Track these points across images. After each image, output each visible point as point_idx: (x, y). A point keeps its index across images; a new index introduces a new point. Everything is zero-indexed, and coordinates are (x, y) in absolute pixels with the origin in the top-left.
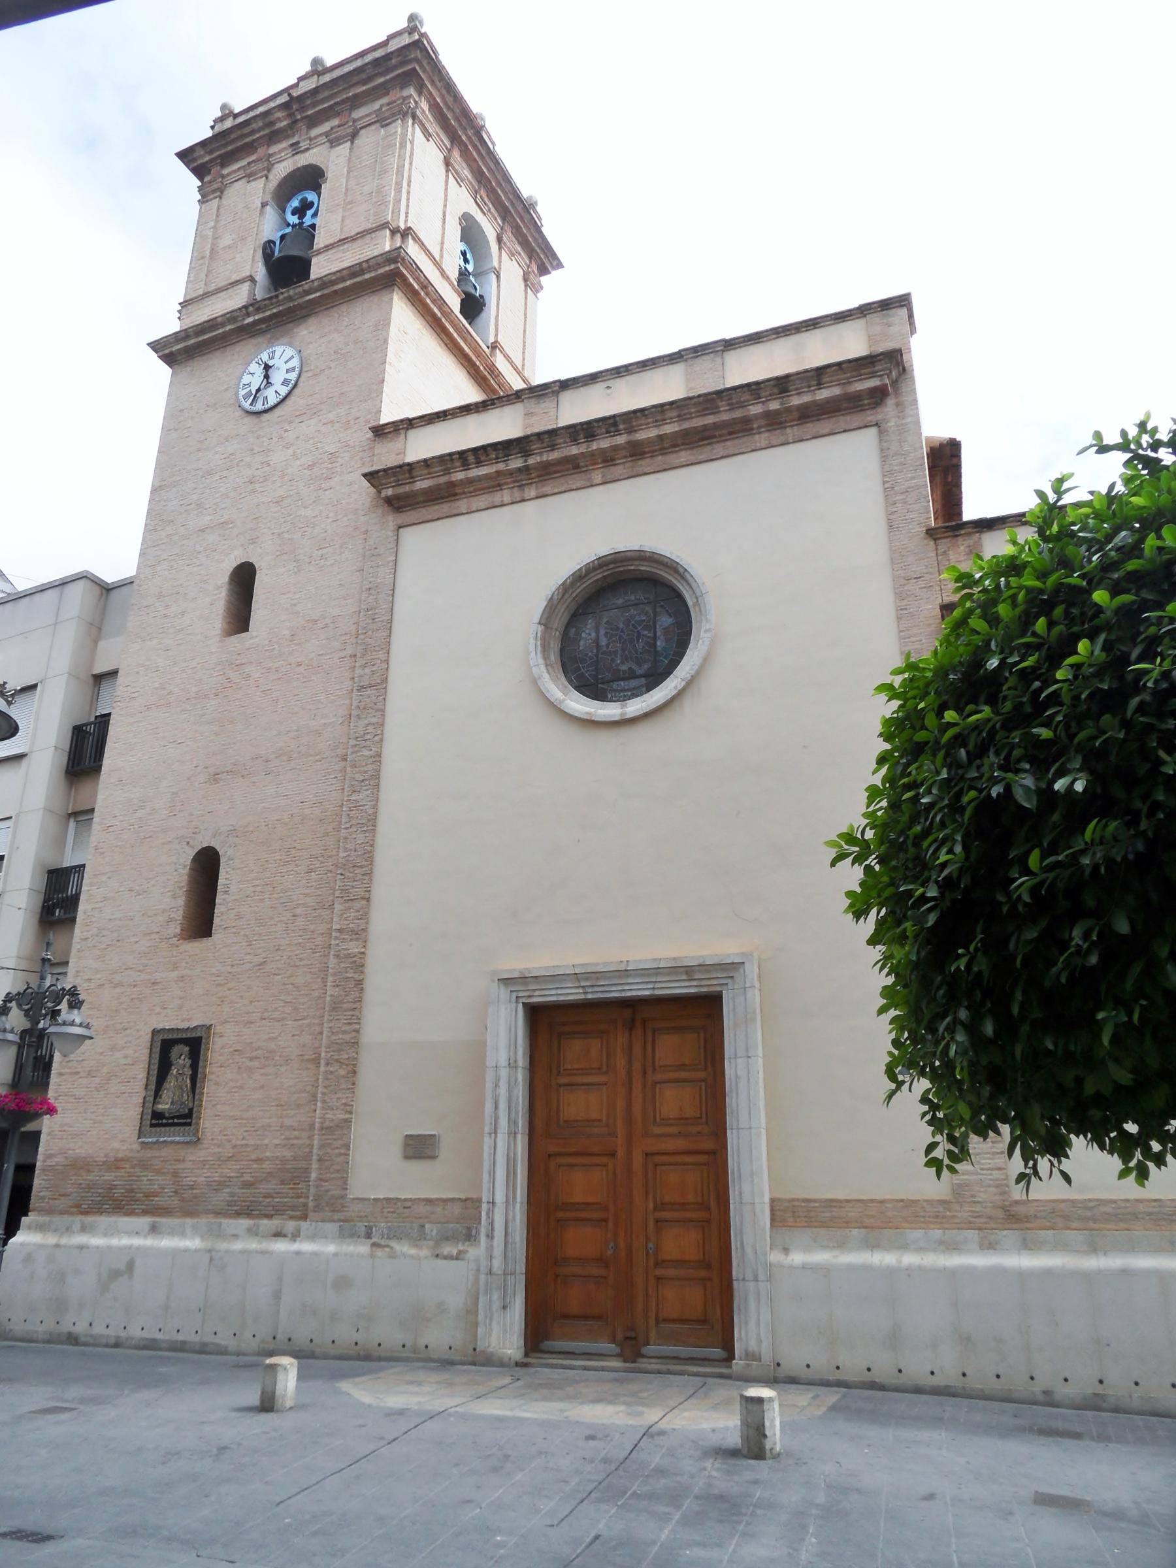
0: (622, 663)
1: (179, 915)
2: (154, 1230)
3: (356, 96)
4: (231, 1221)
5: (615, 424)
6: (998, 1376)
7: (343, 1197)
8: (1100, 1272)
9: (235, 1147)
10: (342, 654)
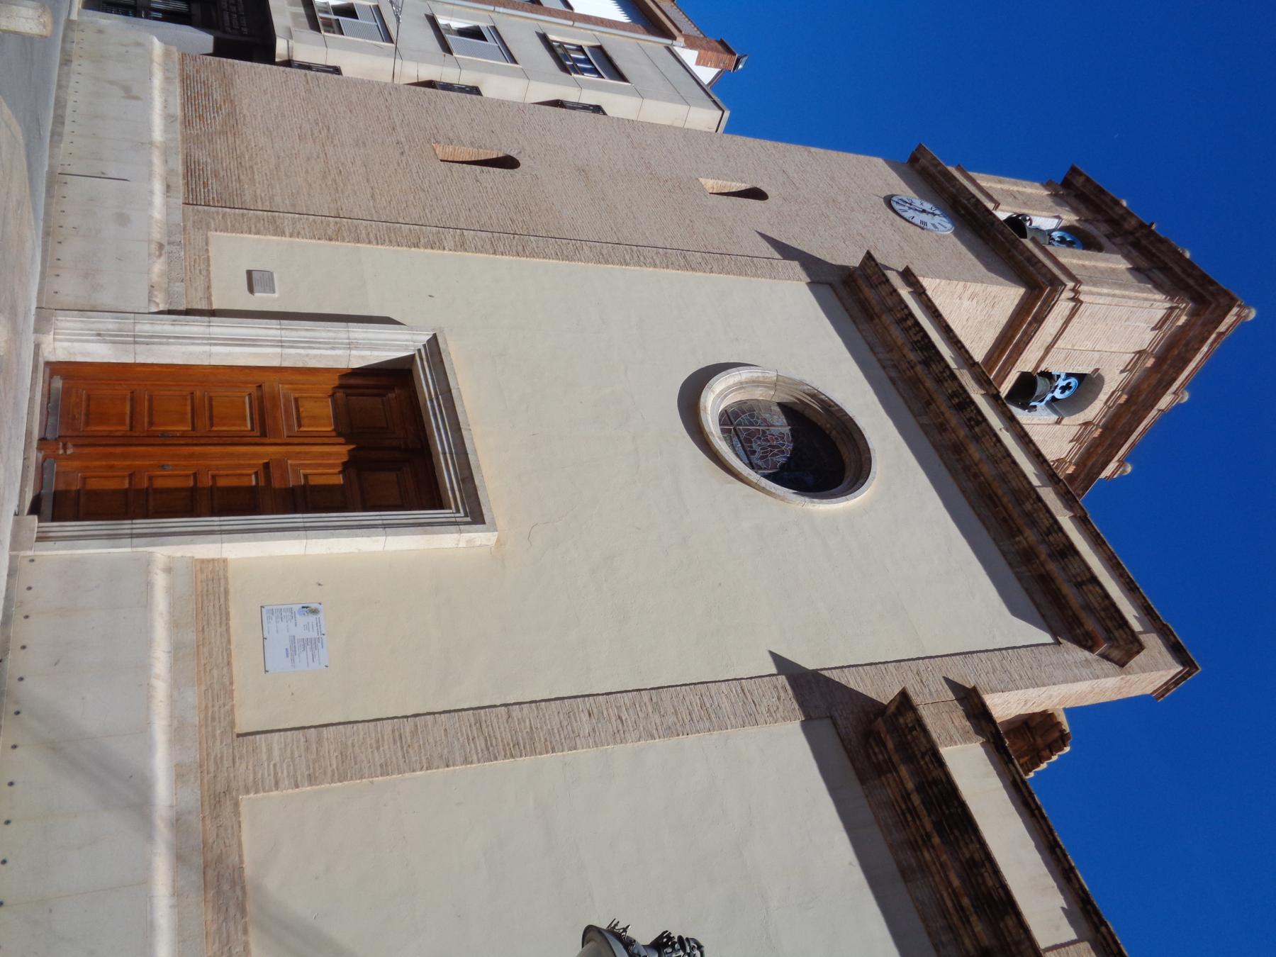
2: (169, 118)
3: (1171, 269)
5: (978, 423)
6: (11, 784)
7: (208, 228)
8: (149, 898)
9: (251, 167)
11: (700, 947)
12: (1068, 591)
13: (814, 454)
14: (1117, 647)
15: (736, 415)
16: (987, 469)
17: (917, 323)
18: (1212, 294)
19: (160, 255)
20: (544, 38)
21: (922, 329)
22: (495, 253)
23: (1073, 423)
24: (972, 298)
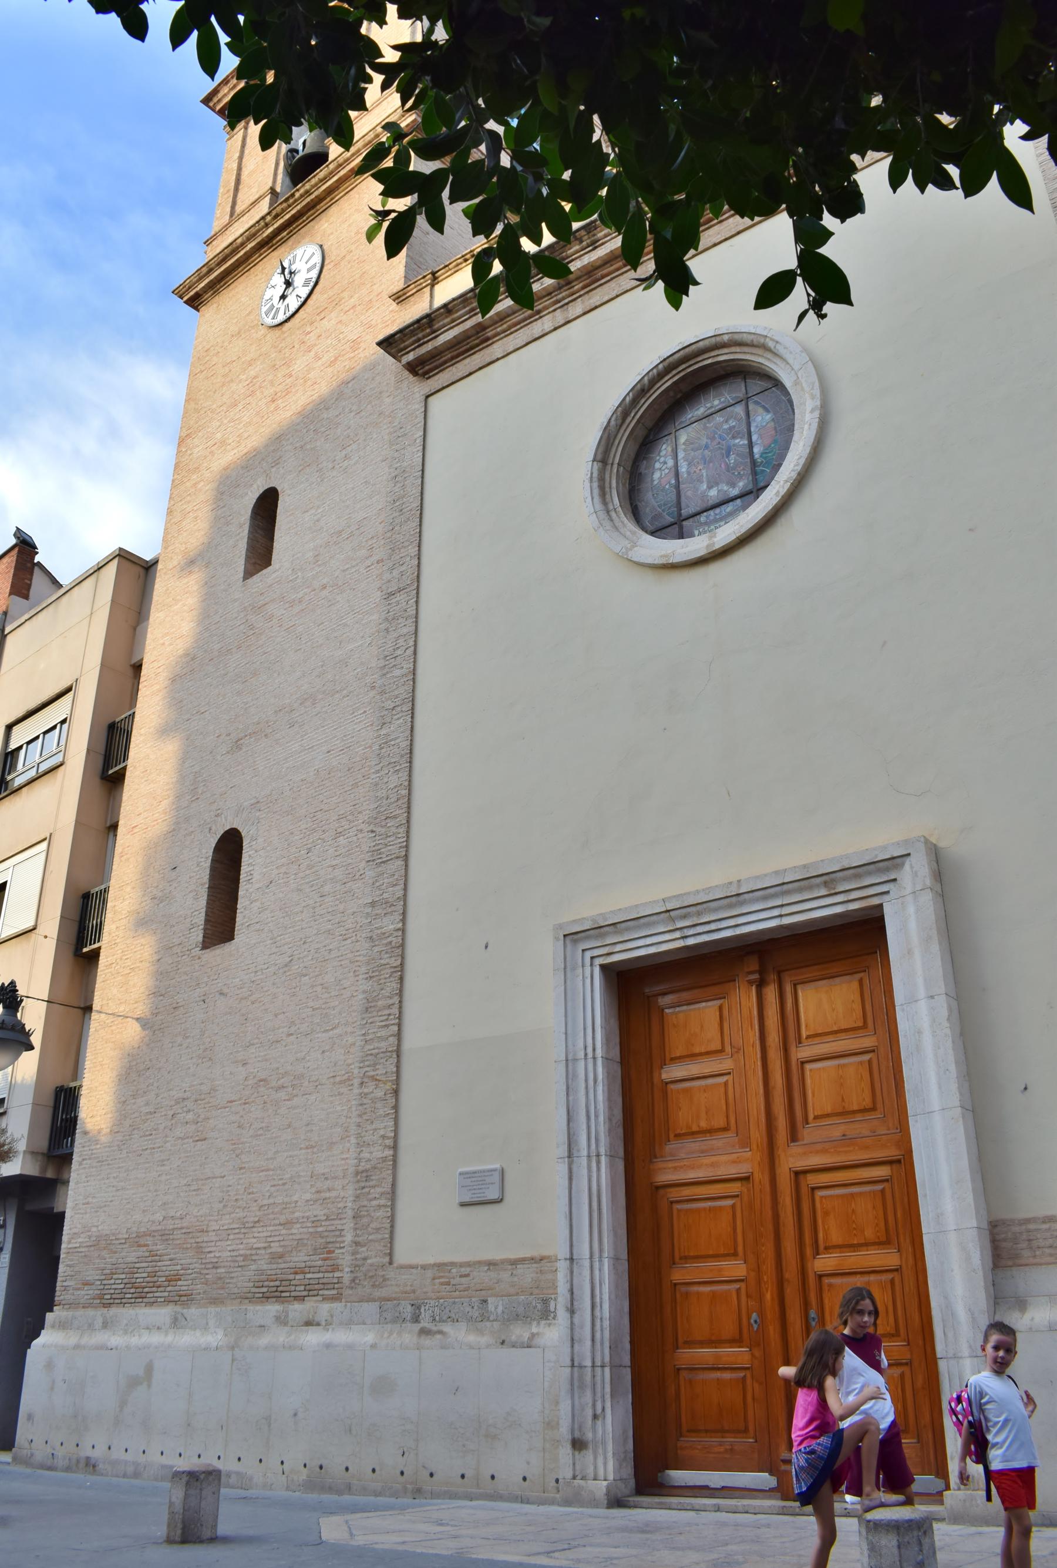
0: (710, 487)
1: (200, 919)
2: (176, 1323)
4: (259, 1308)
10: (368, 562)
11: (1016, 1488)
19: (440, 1332)
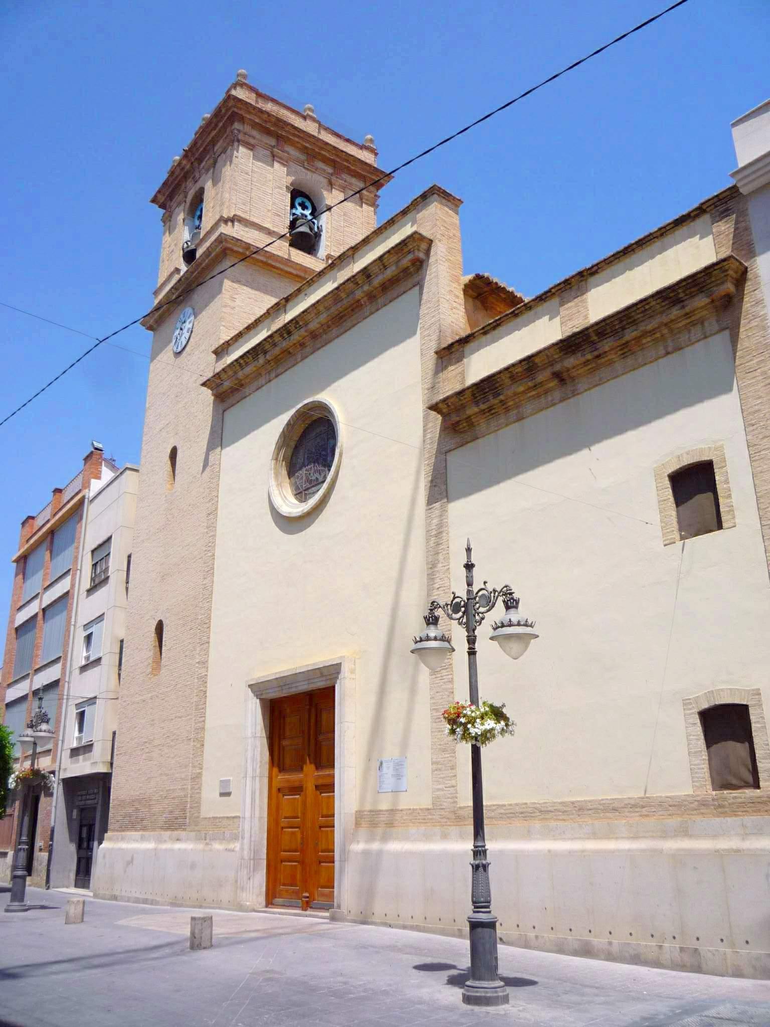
2: (143, 839)
5: (297, 323)
7: (198, 817)
12: (390, 272)
13: (311, 446)
14: (418, 246)
15: (297, 488)
16: (323, 318)
17: (241, 357)
18: (227, 110)
20: (90, 591)
21: (245, 354)
22: (208, 643)
23: (332, 197)
24: (233, 299)
